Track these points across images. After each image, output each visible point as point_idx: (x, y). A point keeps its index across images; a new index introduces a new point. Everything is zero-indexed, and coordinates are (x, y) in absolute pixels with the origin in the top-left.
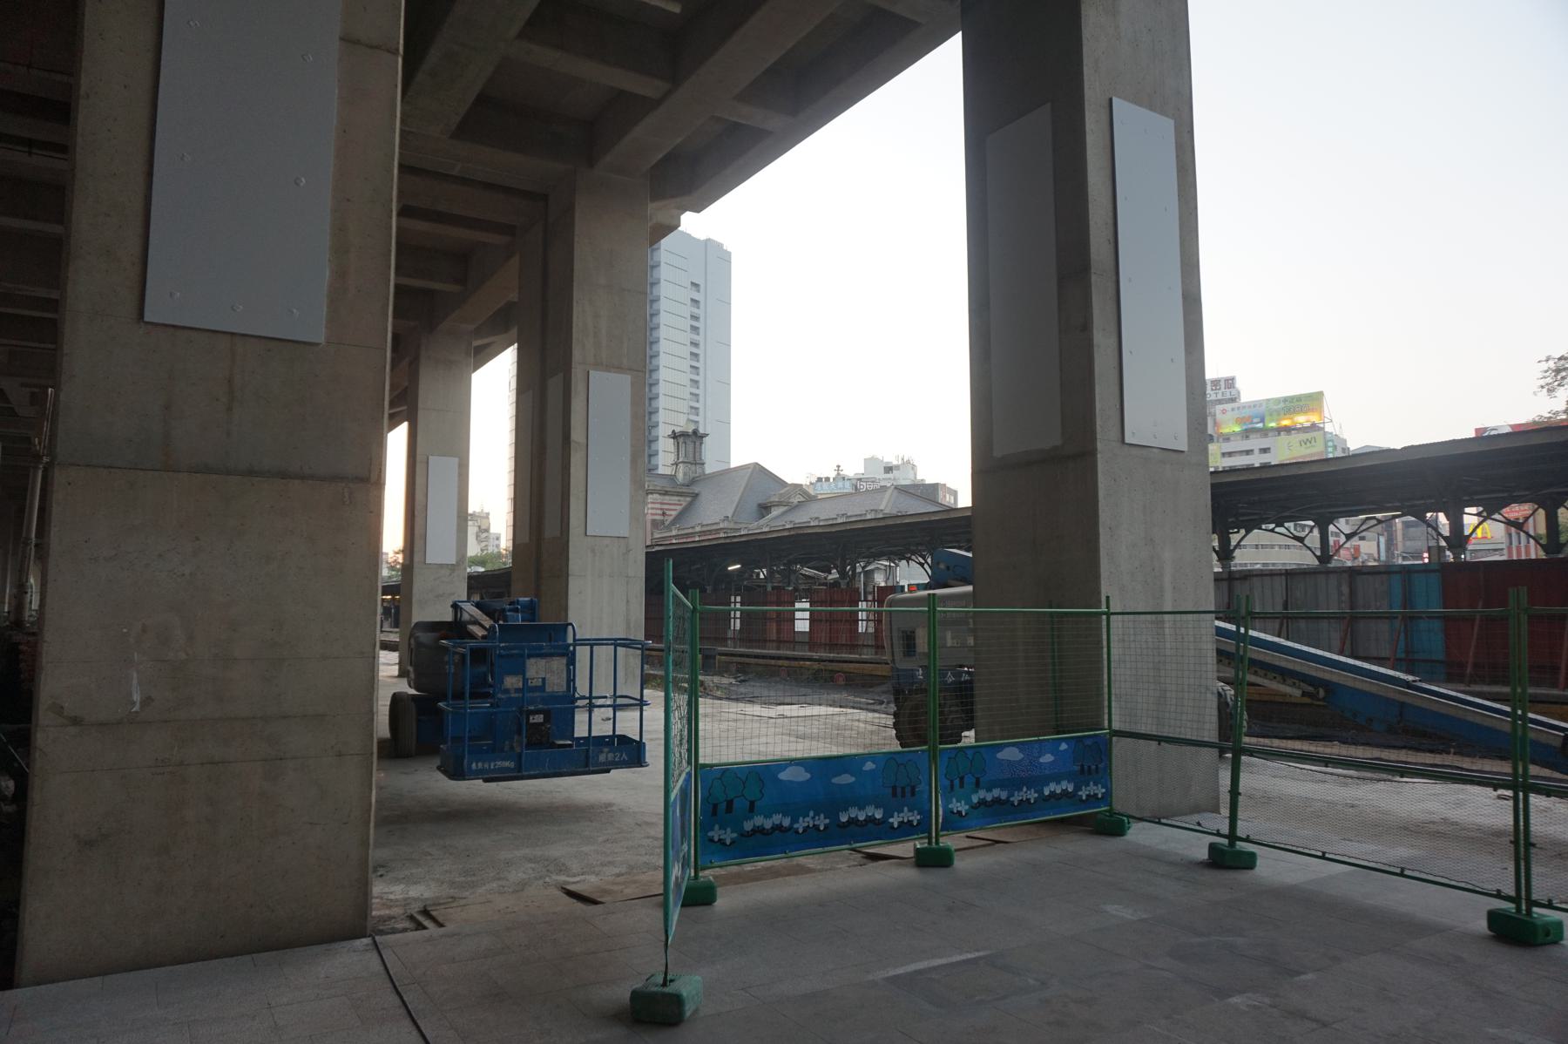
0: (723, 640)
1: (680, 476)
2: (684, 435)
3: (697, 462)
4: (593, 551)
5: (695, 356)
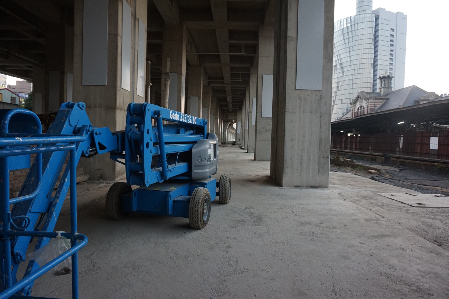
0: (395, 152)
1: (382, 93)
2: (384, 78)
3: (389, 87)
4: (300, 98)
5: (391, 55)
